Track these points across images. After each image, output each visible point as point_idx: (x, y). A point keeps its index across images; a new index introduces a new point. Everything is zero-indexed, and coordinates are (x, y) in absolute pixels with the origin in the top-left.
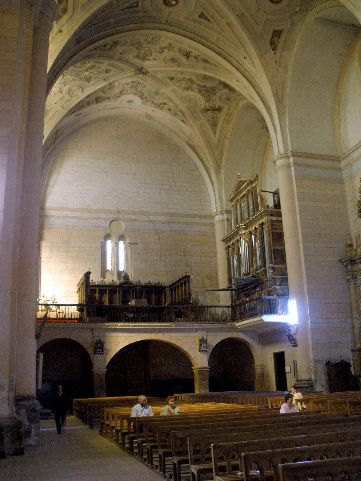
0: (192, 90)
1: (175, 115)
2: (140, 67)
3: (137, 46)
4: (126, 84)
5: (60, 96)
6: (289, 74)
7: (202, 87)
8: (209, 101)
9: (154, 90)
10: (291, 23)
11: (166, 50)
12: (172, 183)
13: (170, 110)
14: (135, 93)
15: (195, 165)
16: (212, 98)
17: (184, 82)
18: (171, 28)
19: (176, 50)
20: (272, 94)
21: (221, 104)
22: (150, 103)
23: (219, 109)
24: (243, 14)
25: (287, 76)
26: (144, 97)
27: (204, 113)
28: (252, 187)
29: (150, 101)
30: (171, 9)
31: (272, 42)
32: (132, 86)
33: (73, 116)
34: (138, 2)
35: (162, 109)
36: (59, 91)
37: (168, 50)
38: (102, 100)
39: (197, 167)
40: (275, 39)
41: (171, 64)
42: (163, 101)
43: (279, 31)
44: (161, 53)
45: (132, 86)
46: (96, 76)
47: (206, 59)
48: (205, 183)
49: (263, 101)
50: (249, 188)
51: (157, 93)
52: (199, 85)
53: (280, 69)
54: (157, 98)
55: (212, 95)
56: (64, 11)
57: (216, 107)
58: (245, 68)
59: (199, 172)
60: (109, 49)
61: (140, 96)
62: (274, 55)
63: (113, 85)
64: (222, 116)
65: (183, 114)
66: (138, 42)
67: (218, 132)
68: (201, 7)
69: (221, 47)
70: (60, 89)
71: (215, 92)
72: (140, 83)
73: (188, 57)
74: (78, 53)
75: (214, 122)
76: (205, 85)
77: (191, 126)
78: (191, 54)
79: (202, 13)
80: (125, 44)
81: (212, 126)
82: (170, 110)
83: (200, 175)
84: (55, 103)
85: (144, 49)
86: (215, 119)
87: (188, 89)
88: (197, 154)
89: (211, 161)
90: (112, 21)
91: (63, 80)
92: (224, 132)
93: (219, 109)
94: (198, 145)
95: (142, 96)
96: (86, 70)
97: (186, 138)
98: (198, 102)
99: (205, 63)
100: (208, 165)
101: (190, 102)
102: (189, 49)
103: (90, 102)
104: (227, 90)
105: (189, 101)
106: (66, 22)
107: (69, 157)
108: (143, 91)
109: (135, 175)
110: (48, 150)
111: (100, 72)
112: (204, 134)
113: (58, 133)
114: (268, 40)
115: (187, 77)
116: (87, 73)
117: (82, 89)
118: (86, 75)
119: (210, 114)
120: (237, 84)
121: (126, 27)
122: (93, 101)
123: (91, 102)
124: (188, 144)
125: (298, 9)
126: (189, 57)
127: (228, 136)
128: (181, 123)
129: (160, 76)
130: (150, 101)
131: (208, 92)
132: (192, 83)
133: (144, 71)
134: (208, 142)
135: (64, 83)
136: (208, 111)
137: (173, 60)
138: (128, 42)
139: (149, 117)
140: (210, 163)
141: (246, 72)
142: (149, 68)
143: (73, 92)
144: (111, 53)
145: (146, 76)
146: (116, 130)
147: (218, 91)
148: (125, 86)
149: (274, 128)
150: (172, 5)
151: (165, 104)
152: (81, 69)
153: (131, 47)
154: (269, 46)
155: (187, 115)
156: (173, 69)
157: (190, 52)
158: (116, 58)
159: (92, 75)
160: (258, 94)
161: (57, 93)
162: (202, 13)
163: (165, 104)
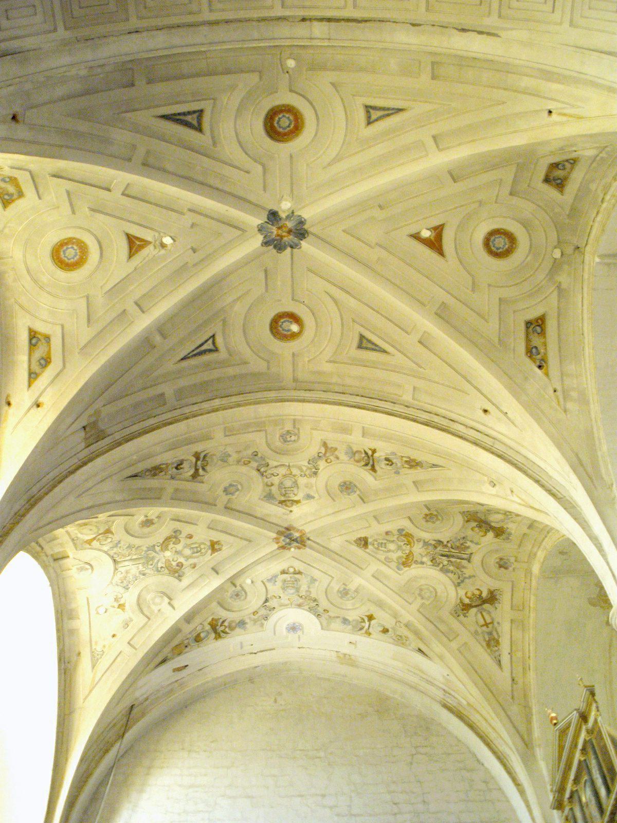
0: (416, 562)
1: (400, 640)
2: (286, 525)
3: (255, 465)
4: (269, 580)
5: (122, 616)
6: (595, 408)
7: (436, 547)
8: (462, 581)
9: (336, 587)
10: (556, 293)
11: (322, 464)
12: (420, 807)
13: (385, 631)
14: (298, 603)
15: (474, 755)
16: (467, 572)
17: (392, 546)
18: (307, 395)
19: (343, 457)
20: (568, 468)
21: (493, 584)
22: (337, 624)
23: (492, 598)
24: (444, 305)
25: (593, 416)
26: (320, 609)
27: (462, 617)
28: (588, 732)
29: (338, 617)
30: (294, 345)
31: (531, 351)
32: (285, 586)
33: (166, 669)
34: (213, 336)
35: (368, 634)
36: (116, 605)
37: (326, 461)
38: (227, 630)
39: (478, 761)
40: (536, 341)
41: (346, 500)
42: (363, 611)
43: (537, 320)
44: (315, 473)
45: (285, 586)
46: (192, 561)
47: (412, 458)
48: (505, 797)
49: (554, 495)
50: (583, 735)
51: (344, 593)
52: (426, 544)
53: (570, 405)
54: (349, 604)
55: (464, 562)
56: (43, 362)
57: (484, 595)
58: (494, 438)
59: (487, 771)
60: (195, 475)
61: (310, 610)
62: (546, 379)
63: (241, 586)
64: (503, 613)
65: (417, 633)
66: (255, 454)
67: (505, 659)
68: (354, 321)
69: (429, 408)
70: (116, 600)
71: (468, 551)
72: (300, 573)
73: (373, 469)
74: (91, 460)
75: (490, 633)
76: (438, 536)
77: (441, 658)
78: (376, 455)
79: (362, 337)
80: (225, 459)
81: (488, 644)
82: (385, 631)
83: (489, 780)
84: (114, 636)
85: (275, 471)
86: (490, 626)
87: (406, 562)
88: (472, 726)
89: (498, 725)
90: (168, 390)
91: (119, 576)
92: (519, 654)
93: (492, 598)
94: (469, 704)
95: (315, 609)
96: (165, 545)
97: (439, 694)
98: (439, 591)
99: (412, 471)
100: (503, 748)
101: (422, 598)
102: (368, 444)
103: (198, 635)
104: (491, 534)
105: (420, 595)
106: (49, 385)
107: (162, 768)
108: (313, 595)
109: (323, 796)
110: (107, 751)
111: (197, 551)
112: (473, 669)
113: (134, 712)
114: (521, 348)
115: (393, 526)
116: (168, 554)
117: (170, 599)
118: (168, 561)
119: (476, 615)
120: (493, 491)
121: (205, 406)
122: (208, 633)
123: (202, 635)
124: (445, 706)
125: (557, 254)
126: (377, 467)
127: (532, 663)
128: (419, 657)
129: (336, 543)
130: (338, 617)
131: (453, 556)
132: (409, 543)
133: (296, 535)
134: (488, 687)
135: (122, 582)
136: (469, 610)
137: (347, 487)
138: (230, 456)
139: (347, 660)
140: (505, 742)
141: (498, 446)
142: (303, 525)
143: (149, 607)
144: (201, 488)
145: (308, 550)
146: (276, 701)
147: (473, 548)
148: (269, 585)
149: (595, 545)
150: (294, 336)
151: (371, 618)
152: (150, 541)
153: (244, 469)
154: (528, 360)
155: (425, 633)
156: (352, 513)
157: (374, 451)
158: (220, 506)
159: (182, 560)
160: (537, 481)
161: (111, 610)
162: (362, 337)
163: (371, 618)
